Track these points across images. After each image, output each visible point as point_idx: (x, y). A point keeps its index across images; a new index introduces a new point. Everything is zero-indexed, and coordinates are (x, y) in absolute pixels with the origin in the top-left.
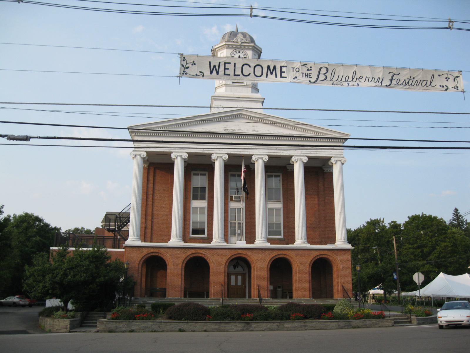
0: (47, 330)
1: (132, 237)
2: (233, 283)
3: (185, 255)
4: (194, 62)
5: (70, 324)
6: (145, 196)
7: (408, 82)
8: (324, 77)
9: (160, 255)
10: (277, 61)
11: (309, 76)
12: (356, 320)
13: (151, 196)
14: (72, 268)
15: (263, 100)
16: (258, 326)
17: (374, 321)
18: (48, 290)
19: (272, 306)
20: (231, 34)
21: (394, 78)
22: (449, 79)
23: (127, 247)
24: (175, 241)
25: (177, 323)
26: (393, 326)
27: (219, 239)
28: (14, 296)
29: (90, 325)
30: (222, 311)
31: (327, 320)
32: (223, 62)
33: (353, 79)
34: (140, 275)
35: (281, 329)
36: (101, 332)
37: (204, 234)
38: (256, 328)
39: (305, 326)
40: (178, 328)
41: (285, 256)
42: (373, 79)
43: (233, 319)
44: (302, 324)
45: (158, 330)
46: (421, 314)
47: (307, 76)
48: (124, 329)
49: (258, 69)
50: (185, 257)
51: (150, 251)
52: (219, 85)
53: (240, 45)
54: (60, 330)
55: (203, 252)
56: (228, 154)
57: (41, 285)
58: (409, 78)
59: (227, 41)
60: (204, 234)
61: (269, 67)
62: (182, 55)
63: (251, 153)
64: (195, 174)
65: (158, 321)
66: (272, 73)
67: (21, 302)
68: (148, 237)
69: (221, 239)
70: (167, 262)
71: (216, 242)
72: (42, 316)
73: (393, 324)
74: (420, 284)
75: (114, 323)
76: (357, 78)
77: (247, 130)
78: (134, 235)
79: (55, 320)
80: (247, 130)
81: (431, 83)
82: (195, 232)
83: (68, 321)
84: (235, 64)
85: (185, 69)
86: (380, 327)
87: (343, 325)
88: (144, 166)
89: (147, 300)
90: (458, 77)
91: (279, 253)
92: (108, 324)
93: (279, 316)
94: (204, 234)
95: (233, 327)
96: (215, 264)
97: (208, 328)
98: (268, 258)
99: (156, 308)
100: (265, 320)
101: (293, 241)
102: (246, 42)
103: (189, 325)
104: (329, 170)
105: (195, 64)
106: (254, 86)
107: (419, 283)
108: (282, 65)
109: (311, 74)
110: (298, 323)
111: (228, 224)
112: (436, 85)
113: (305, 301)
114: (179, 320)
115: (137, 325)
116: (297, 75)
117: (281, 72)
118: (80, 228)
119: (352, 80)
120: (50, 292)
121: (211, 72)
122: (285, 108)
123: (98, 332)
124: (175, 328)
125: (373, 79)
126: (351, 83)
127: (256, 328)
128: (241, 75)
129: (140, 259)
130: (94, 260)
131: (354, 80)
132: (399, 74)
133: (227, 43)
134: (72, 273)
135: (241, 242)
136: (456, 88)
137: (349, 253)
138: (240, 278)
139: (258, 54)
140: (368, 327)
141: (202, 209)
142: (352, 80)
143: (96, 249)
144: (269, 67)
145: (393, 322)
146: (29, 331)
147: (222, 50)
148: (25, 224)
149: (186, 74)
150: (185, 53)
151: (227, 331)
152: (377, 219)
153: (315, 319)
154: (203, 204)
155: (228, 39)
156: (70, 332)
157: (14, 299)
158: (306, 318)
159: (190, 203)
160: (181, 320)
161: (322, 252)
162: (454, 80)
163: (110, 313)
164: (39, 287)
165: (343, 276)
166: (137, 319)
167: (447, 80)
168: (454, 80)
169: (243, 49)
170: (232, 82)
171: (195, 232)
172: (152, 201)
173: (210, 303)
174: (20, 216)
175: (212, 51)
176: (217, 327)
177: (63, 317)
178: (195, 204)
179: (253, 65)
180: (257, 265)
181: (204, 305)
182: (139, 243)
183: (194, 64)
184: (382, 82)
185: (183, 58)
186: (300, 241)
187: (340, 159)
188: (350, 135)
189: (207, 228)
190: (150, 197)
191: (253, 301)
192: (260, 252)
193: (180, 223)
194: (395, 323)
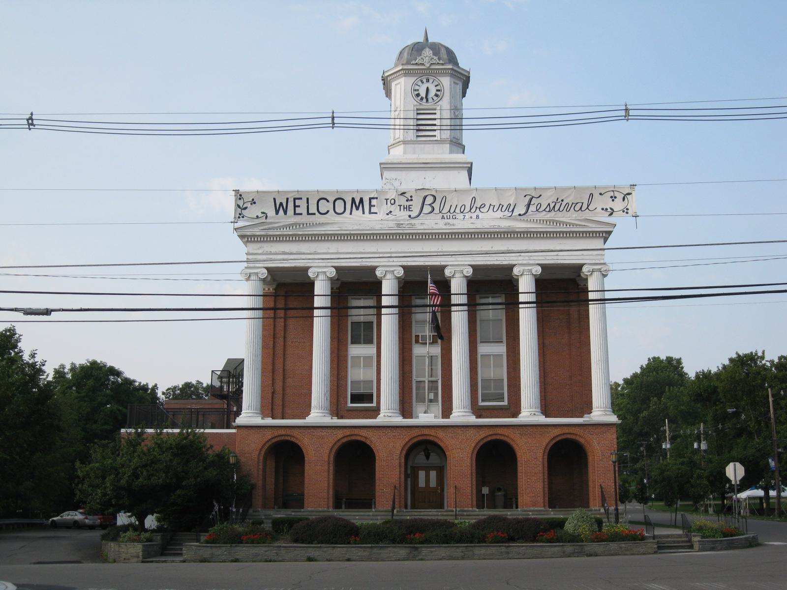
0: (111, 560)
1: (248, 411)
2: (422, 483)
4: (253, 200)
5: (143, 551)
6: (272, 339)
7: (554, 207)
8: (430, 209)
9: (293, 439)
10: (364, 192)
11: (409, 208)
12: (594, 543)
13: (282, 339)
14: (145, 466)
15: (469, 165)
16: (432, 552)
17: (623, 545)
18: (110, 500)
19: (467, 521)
20: (412, 50)
21: (532, 203)
22: (615, 197)
23: (238, 427)
24: (318, 415)
25: (305, 549)
26: (655, 553)
27: (390, 411)
28: (76, 510)
29: (172, 552)
30: (377, 529)
31: (546, 543)
32: (291, 197)
33: (471, 209)
34: (261, 473)
35: (468, 557)
39: (508, 553)
40: (306, 555)
41: (502, 438)
42: (501, 206)
43: (394, 541)
44: (504, 549)
46: (712, 534)
47: (405, 209)
48: (224, 557)
49: (339, 203)
51: (276, 434)
53: (428, 69)
55: (364, 433)
56: (403, 267)
57: (99, 491)
58: (556, 201)
59: (405, 62)
61: (353, 200)
62: (237, 191)
63: (443, 263)
64: (352, 299)
65: (276, 545)
66: (357, 209)
67: (87, 521)
68: (278, 409)
70: (304, 451)
71: (384, 416)
72: (107, 540)
73: (656, 550)
74: (738, 483)
75: (209, 549)
76: (476, 208)
77: (436, 224)
79: (121, 545)
80: (436, 224)
81: (588, 206)
82: (356, 398)
83: (140, 546)
84: (308, 199)
85: (243, 211)
86: (633, 554)
87: (571, 552)
88: (264, 289)
89: (272, 514)
90: (629, 194)
91: (491, 433)
92: (200, 550)
93: (467, 537)
95: (391, 555)
97: (353, 556)
98: (472, 442)
99: (279, 526)
100: (443, 543)
101: (516, 413)
102: (438, 63)
105: (255, 203)
106: (454, 140)
107: (736, 481)
108: (372, 196)
109: (412, 205)
110: (495, 548)
111: (411, 383)
112: (596, 208)
113: (536, 513)
114: (309, 543)
115: (242, 551)
116: (392, 208)
117: (371, 206)
118: (194, 382)
119: (470, 211)
120: (113, 503)
121: (277, 212)
122: (498, 187)
123: (184, 562)
125: (501, 206)
126: (468, 216)
128: (317, 213)
129: (260, 447)
130: (180, 452)
131: (473, 210)
132: (540, 195)
133: (405, 67)
134: (145, 473)
135: (427, 415)
136: (626, 211)
137: (614, 430)
138: (433, 474)
139: (463, 81)
140: (612, 555)
141: (368, 358)
142: (470, 211)
143: (190, 430)
144: (353, 200)
145: (656, 546)
146: (83, 561)
148: (90, 382)
149: (243, 217)
150: (242, 189)
151: (383, 560)
152: (752, 353)
153: (526, 541)
154: (370, 350)
155: (407, 59)
156: (143, 562)
157: (76, 515)
158: (512, 539)
159: (347, 350)
160: (312, 544)
161: (566, 430)
162: (624, 200)
163: (206, 534)
164: (96, 494)
165: (602, 470)
166: (244, 542)
167: (613, 200)
168: (624, 200)
170: (415, 136)
171: (356, 398)
172: (282, 347)
173: (374, 518)
174: (82, 367)
175: (382, 80)
176: (366, 553)
177: (133, 541)
178: (356, 351)
179: (331, 199)
182: (258, 421)
183: (253, 202)
184: (513, 211)
185: (239, 195)
186: (530, 412)
189: (376, 391)
190: (280, 341)
191: (445, 513)
192: (459, 431)
193: (325, 386)
194: (659, 548)
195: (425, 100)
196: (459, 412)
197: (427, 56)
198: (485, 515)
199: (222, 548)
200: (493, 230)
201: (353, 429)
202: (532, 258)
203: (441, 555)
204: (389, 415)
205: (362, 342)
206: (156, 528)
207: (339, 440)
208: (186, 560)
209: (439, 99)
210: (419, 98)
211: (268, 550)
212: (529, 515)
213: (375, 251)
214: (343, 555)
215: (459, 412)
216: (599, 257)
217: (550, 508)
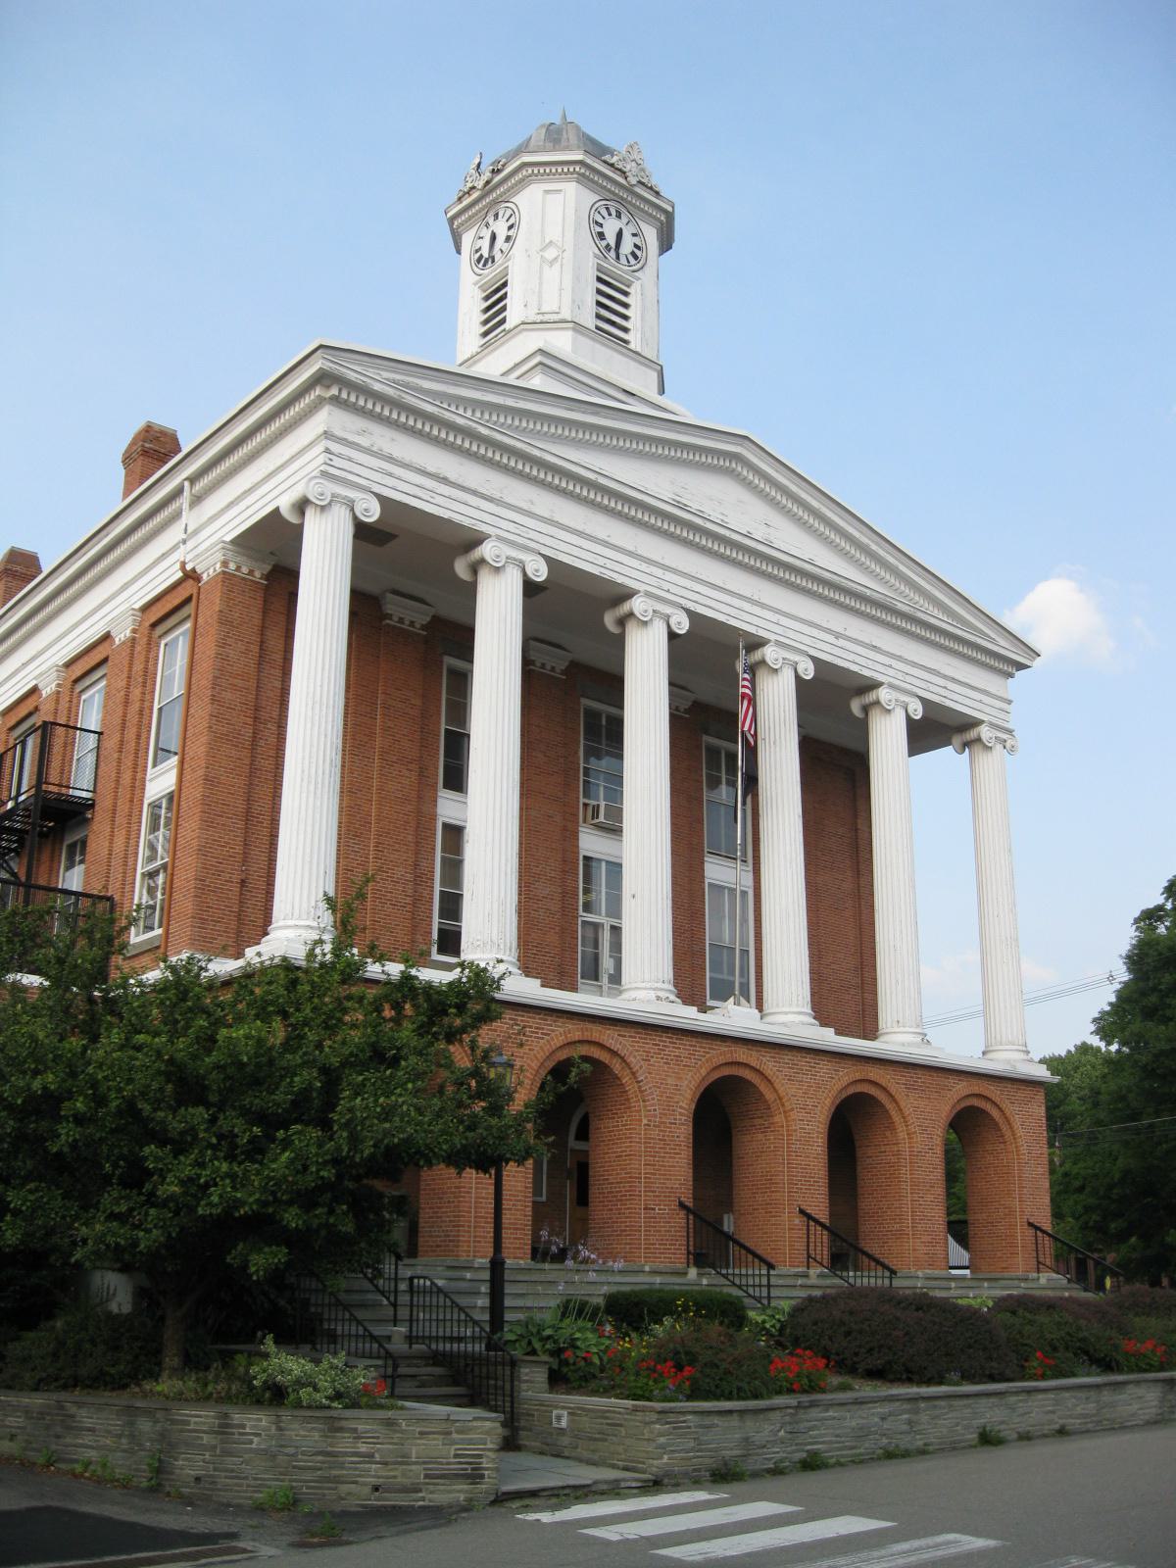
48: (776, 1453)
52: (539, 318)
53: (629, 190)
54: (420, 1491)
71: (658, 998)
169: (628, 206)
187: (1005, 736)
195: (613, 253)
198: (792, 1298)
200: (859, 587)
201: (589, 1026)
206: (269, 1345)
208: (667, 1475)
209: (639, 266)
210: (604, 243)
216: (1002, 715)
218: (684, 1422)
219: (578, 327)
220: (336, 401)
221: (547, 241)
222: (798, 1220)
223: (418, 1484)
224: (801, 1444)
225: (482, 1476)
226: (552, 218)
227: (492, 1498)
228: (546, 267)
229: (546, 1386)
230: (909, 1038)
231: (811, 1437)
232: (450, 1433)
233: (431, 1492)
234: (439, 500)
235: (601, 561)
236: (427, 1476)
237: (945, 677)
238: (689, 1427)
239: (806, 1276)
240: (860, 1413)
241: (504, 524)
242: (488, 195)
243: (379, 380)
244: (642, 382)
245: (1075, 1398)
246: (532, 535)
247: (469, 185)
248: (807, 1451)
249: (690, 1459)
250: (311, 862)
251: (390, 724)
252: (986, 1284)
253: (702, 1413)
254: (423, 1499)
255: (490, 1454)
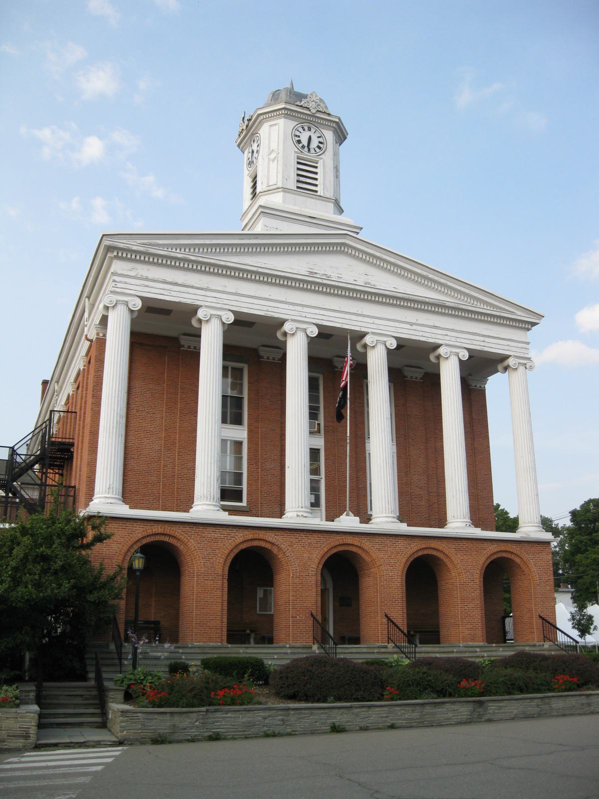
3: (230, 544)
16: (500, 708)
35: (545, 714)
36: (132, 744)
37: (240, 499)
38: (497, 713)
39: (589, 705)
44: (584, 700)
45: (282, 732)
48: (194, 732)
50: (230, 548)
51: (150, 532)
52: (269, 188)
53: (313, 116)
54: (5, 742)
55: (270, 536)
60: (240, 499)
63: (363, 329)
69: (306, 510)
71: (298, 516)
78: (111, 490)
80: (355, 280)
94: (240, 500)
96: (297, 565)
102: (325, 113)
103: (353, 714)
104: (478, 386)
124: (322, 724)
127: (497, 713)
129: (125, 548)
133: (288, 107)
147: (277, 119)
160: (325, 701)
169: (316, 124)
176: (416, 715)
180: (383, 570)
181: (352, 660)
186: (205, 506)
187: (525, 362)
188: (543, 317)
192: (388, 541)
195: (306, 149)
196: (386, 517)
197: (314, 101)
199: (191, 715)
200: (422, 298)
201: (257, 532)
202: (459, 340)
203: (512, 712)
204: (304, 516)
205: (229, 421)
207: (237, 546)
208: (125, 740)
209: (322, 152)
210: (301, 145)
211: (269, 716)
212: (476, 652)
213: (284, 300)
214: (384, 719)
215: (386, 517)
216: (524, 351)
217: (228, 642)
218: (137, 716)
219: (285, 190)
220: (117, 257)
221: (271, 150)
222: (385, 620)
223: (5, 739)
224: (209, 729)
225: (29, 737)
226: (276, 135)
227: (33, 746)
228: (271, 163)
229: (123, 700)
230: (459, 524)
231: (215, 725)
232: (17, 718)
233: (10, 743)
234: (173, 294)
235: (265, 308)
236: (8, 736)
237: (483, 336)
238: (139, 719)
239: (386, 647)
240: (248, 715)
241: (210, 299)
242: (249, 132)
243: (134, 245)
244: (326, 211)
245: (404, 710)
246: (226, 302)
247: (241, 128)
248: (213, 732)
249: (139, 733)
250: (107, 468)
251: (184, 396)
252: (501, 649)
253: (147, 713)
254: (6, 745)
255: (33, 727)
